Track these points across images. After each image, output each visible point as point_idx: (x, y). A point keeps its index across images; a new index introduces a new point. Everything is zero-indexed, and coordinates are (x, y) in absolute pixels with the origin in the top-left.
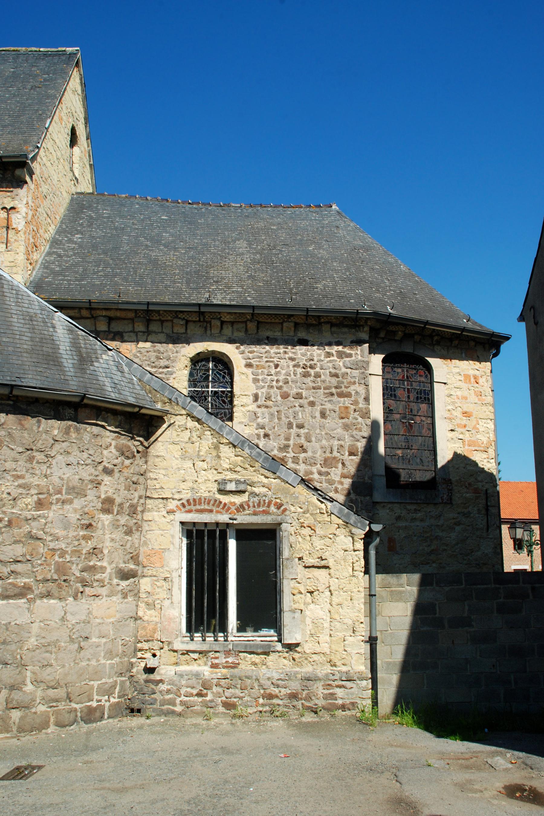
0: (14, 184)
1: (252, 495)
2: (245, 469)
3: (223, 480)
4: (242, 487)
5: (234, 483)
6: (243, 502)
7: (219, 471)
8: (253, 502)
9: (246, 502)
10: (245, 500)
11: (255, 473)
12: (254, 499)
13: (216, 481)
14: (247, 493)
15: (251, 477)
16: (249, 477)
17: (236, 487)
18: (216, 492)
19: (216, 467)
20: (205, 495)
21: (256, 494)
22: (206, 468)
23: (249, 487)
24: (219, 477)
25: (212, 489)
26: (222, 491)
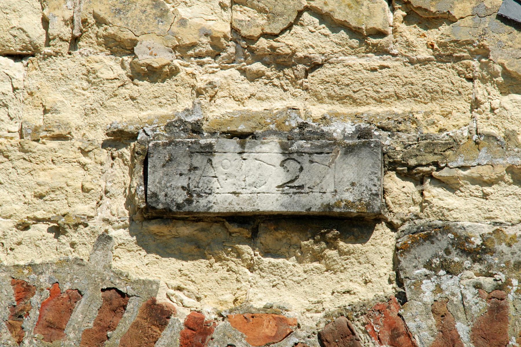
0: (353, 240)
1: (426, 251)
2: (368, 38)
3: (175, 125)
4: (338, 184)
5: (270, 151)
6: (350, 312)
7: (144, 58)
8: (440, 312)
9: (380, 308)
10: (365, 294)
11: (445, 75)
12: (449, 283)
13: (118, 138)
14: (383, 240)
15: (419, 109)
16: (399, 108)
17: (292, 186)
18: (120, 234)
19: (118, 28)
20: (24, 256)
21: (461, 244)
22: (37, 34)
23: (399, 188)
24: (149, 109)
25: (82, 208)
26: (168, 222)
